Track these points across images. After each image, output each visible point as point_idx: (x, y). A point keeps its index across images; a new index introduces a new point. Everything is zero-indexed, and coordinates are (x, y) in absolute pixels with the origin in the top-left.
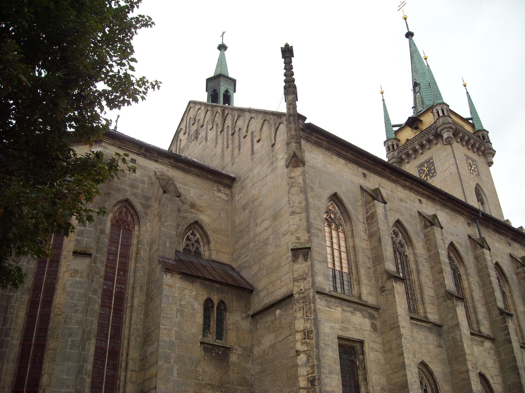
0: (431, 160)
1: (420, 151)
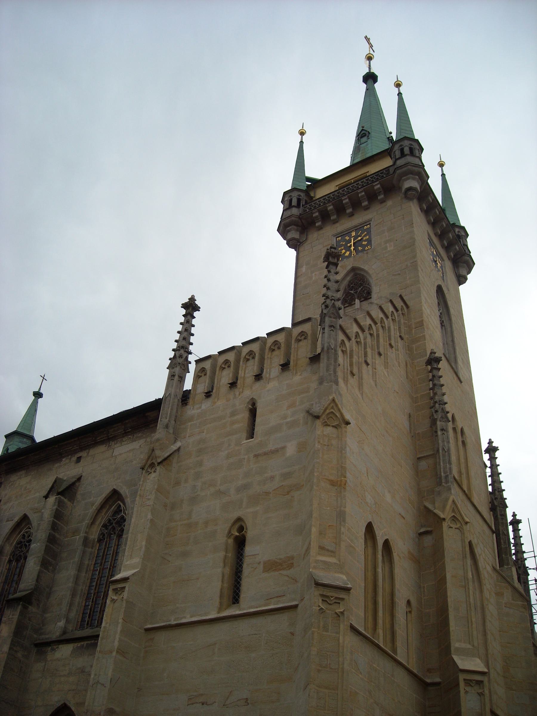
0: (367, 225)
1: (365, 203)
